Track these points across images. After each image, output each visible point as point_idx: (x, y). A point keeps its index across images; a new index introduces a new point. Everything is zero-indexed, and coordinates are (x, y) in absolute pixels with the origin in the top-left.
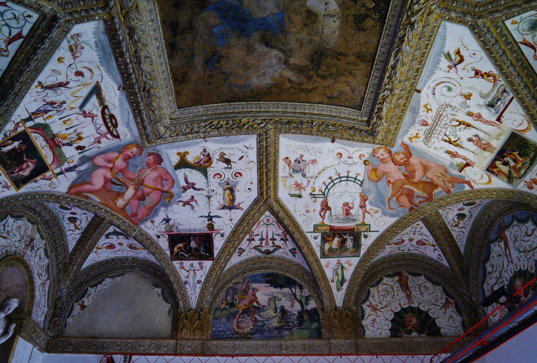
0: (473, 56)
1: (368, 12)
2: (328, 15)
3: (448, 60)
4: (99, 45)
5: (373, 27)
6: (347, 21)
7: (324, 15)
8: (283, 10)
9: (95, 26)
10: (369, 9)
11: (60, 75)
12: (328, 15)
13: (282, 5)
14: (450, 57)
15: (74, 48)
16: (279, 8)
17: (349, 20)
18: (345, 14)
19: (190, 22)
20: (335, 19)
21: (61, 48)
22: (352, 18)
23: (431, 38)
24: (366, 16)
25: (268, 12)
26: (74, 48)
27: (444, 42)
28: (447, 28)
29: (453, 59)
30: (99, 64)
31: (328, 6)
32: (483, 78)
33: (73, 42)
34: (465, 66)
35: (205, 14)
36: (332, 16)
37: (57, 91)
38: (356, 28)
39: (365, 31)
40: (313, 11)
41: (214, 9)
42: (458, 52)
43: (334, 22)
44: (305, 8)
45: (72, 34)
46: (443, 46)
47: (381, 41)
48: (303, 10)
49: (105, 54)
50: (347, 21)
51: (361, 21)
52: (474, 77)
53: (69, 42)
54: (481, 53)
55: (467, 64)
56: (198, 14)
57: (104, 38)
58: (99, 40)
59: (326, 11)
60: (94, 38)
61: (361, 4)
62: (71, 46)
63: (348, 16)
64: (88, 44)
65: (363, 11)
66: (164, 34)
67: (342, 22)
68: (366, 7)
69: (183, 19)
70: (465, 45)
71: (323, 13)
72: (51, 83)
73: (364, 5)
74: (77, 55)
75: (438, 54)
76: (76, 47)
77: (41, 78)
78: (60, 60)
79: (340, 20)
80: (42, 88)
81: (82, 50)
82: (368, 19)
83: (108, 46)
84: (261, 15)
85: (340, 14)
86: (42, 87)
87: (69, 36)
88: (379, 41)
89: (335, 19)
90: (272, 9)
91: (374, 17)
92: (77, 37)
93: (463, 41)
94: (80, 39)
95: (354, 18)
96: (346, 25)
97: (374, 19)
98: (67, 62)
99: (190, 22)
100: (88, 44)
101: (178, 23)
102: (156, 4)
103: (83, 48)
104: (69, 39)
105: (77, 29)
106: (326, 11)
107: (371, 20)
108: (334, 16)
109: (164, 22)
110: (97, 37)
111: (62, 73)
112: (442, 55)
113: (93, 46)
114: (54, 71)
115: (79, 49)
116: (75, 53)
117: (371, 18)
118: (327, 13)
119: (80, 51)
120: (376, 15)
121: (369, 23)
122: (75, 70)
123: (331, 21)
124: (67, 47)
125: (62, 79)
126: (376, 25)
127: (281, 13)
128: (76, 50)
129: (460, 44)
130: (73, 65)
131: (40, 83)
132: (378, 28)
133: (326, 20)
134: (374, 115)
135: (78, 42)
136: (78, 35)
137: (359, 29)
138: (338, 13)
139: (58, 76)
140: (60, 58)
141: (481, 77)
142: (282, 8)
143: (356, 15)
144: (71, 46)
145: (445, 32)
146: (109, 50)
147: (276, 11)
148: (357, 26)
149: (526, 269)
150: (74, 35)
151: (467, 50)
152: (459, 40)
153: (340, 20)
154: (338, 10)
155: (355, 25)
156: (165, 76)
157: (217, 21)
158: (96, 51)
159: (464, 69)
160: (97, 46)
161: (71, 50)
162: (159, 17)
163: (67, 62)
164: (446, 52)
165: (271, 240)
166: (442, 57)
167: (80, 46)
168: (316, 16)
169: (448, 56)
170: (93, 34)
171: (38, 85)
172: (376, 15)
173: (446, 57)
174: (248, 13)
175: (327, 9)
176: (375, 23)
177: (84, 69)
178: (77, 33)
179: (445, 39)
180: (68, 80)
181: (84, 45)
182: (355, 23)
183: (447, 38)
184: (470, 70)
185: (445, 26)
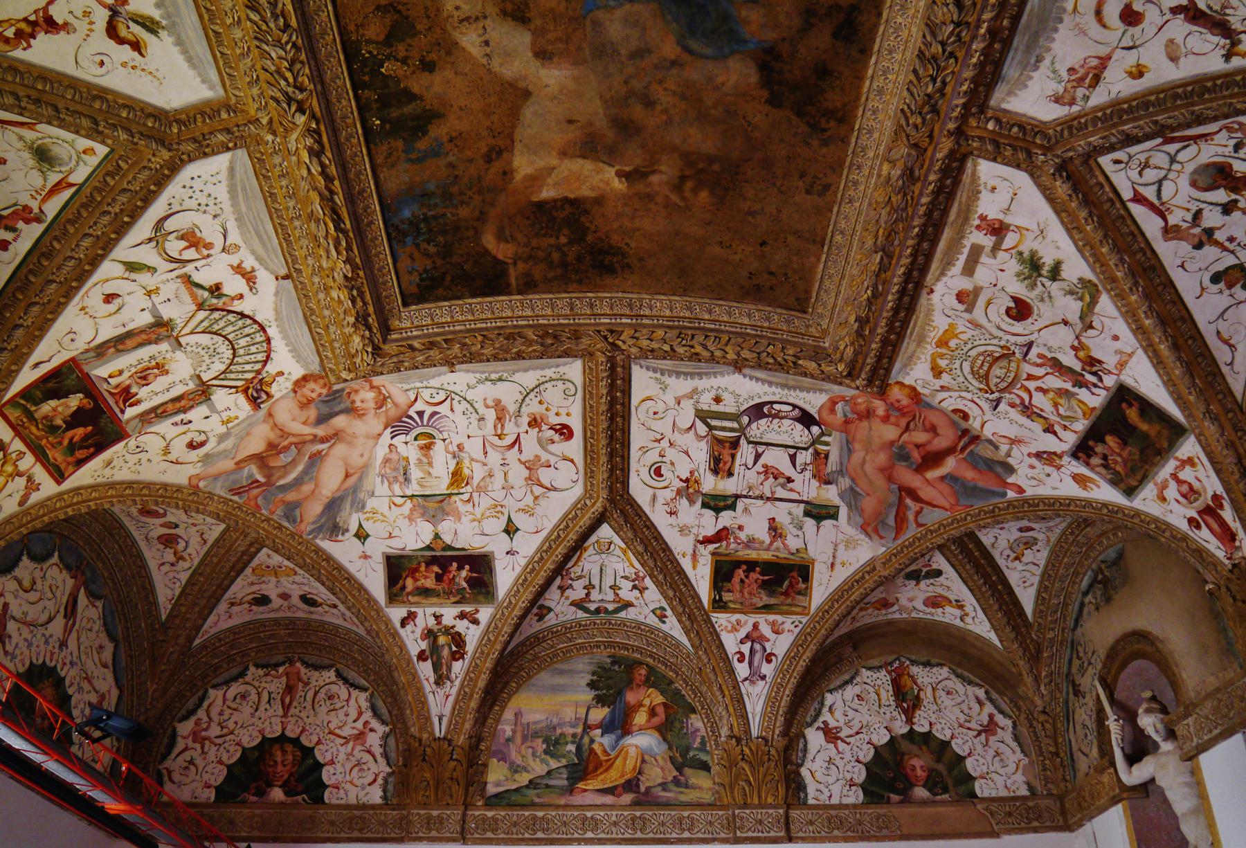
0: (98, 59)
1: (388, 51)
2: (477, 18)
3: (141, 17)
4: (1033, 60)
5: (362, 25)
6: (428, 17)
7: (485, 17)
8: (585, 18)
9: (1012, 99)
10: (388, 58)
11: (1171, 41)
12: (477, 18)
13: (589, 29)
14: (143, 26)
15: (1087, 81)
16: (595, 23)
17: (425, 21)
18: (439, 31)
19: (807, 27)
20: (456, 14)
21: (1113, 95)
22: (419, 27)
23: (214, 40)
24: (388, 41)
25: (619, 13)
26: (1087, 81)
27: (185, 52)
28: (204, 86)
29: (131, 24)
30: (1066, 18)
31: (482, 39)
32: (25, 20)
33: (1080, 92)
34: (92, 23)
35: (770, 35)
36: (467, 19)
37: (1217, 7)
38: (400, 7)
39: (378, 8)
40: (513, 23)
41: (745, 42)
42: (136, 46)
43: (457, 8)
44: (532, 26)
45: (1067, 108)
46: (179, 42)
47: (330, 8)
48: (538, 22)
49: (1036, 36)
50: (428, 17)
51: (393, 27)
52: (45, 9)
53: (1086, 98)
54: (89, 73)
55: (91, 30)
56: (784, 39)
57: (1011, 70)
58: (1024, 69)
59: (484, 27)
60: (1031, 78)
61: (410, 62)
62: (1090, 86)
63: (429, 29)
64: (1054, 72)
65: (401, 50)
66: (876, 26)
67: (438, 10)
68: (397, 60)
69: (821, 40)
70: (138, 72)
71: (488, 22)
72: (1209, 37)
73: (404, 61)
74: (1094, 62)
75: (177, 20)
76: (1082, 79)
77: (1214, 64)
78: (1138, 72)
79: (445, 14)
80: (1240, 42)
81: (1076, 67)
82: (382, 37)
83: (1016, 49)
84: (637, 7)
85: (449, 28)
86: (1235, 43)
87: (1075, 109)
88: (371, 160)
89: (456, 14)
90: (611, 21)
91: (370, 48)
92: (1062, 97)
93: (150, 77)
94: (1061, 90)
95: (414, 27)
96: (426, 8)
97: (369, 41)
98: (1131, 59)
99: (807, 27)
100: (1054, 72)
101: (836, 35)
102: (865, 90)
103: (1071, 70)
104: (1081, 103)
105: (1049, 113)
106: (484, 27)
107: (374, 37)
108: (461, 21)
109: (865, 52)
110: (1023, 78)
111: (1164, 41)
112: (164, 23)
113: (1047, 62)
114: (1174, 59)
115: (1081, 72)
116: (1095, 68)
117: (377, 43)
118: (481, 25)
119: (1082, 66)
120: (370, 52)
121: (375, 30)
122: (1132, 30)
123: (465, 7)
124: (1101, 88)
125: (1179, 28)
126: (357, 31)
127: (591, 11)
128: (1088, 74)
129: (151, 68)
130: (1124, 43)
131: (1228, 57)
132: (352, 28)
133: (479, 6)
134: (312, 87)
135: (1069, 85)
136: (1058, 100)
137: (395, 8)
138: (455, 28)
139: (1179, 40)
140: (1134, 78)
141: (33, 18)
142: (588, 22)
143: (414, 36)
144: (1090, 86)
145: (200, 75)
146: (1019, 41)
147: (600, 14)
148: (399, 12)
149: (53, 664)
150: (1064, 104)
151: (124, 65)
152: (158, 74)
153: (445, 14)
154: (456, 35)
155: (405, 13)
156: (846, 208)
157: (744, 13)
158: (1049, 49)
159: (87, 14)
160: (1039, 60)
161: (1097, 79)
162: (870, 72)
163: (1131, 59)
164: (163, 34)
165: (594, 587)
166: (162, 17)
167: (1073, 77)
168: (504, 13)
169: (151, 26)
170: (1026, 86)
171: (1237, 54)
172: (370, 52)
173: (152, 20)
174: (669, 17)
175: (481, 32)
176: (363, 35)
177: (1106, 20)
178: (1057, 106)
179: (190, 60)
180: (1169, 16)
181: (1065, 75)
182: (407, 18)
183: (186, 65)
184: (71, 19)
185: (212, 88)
